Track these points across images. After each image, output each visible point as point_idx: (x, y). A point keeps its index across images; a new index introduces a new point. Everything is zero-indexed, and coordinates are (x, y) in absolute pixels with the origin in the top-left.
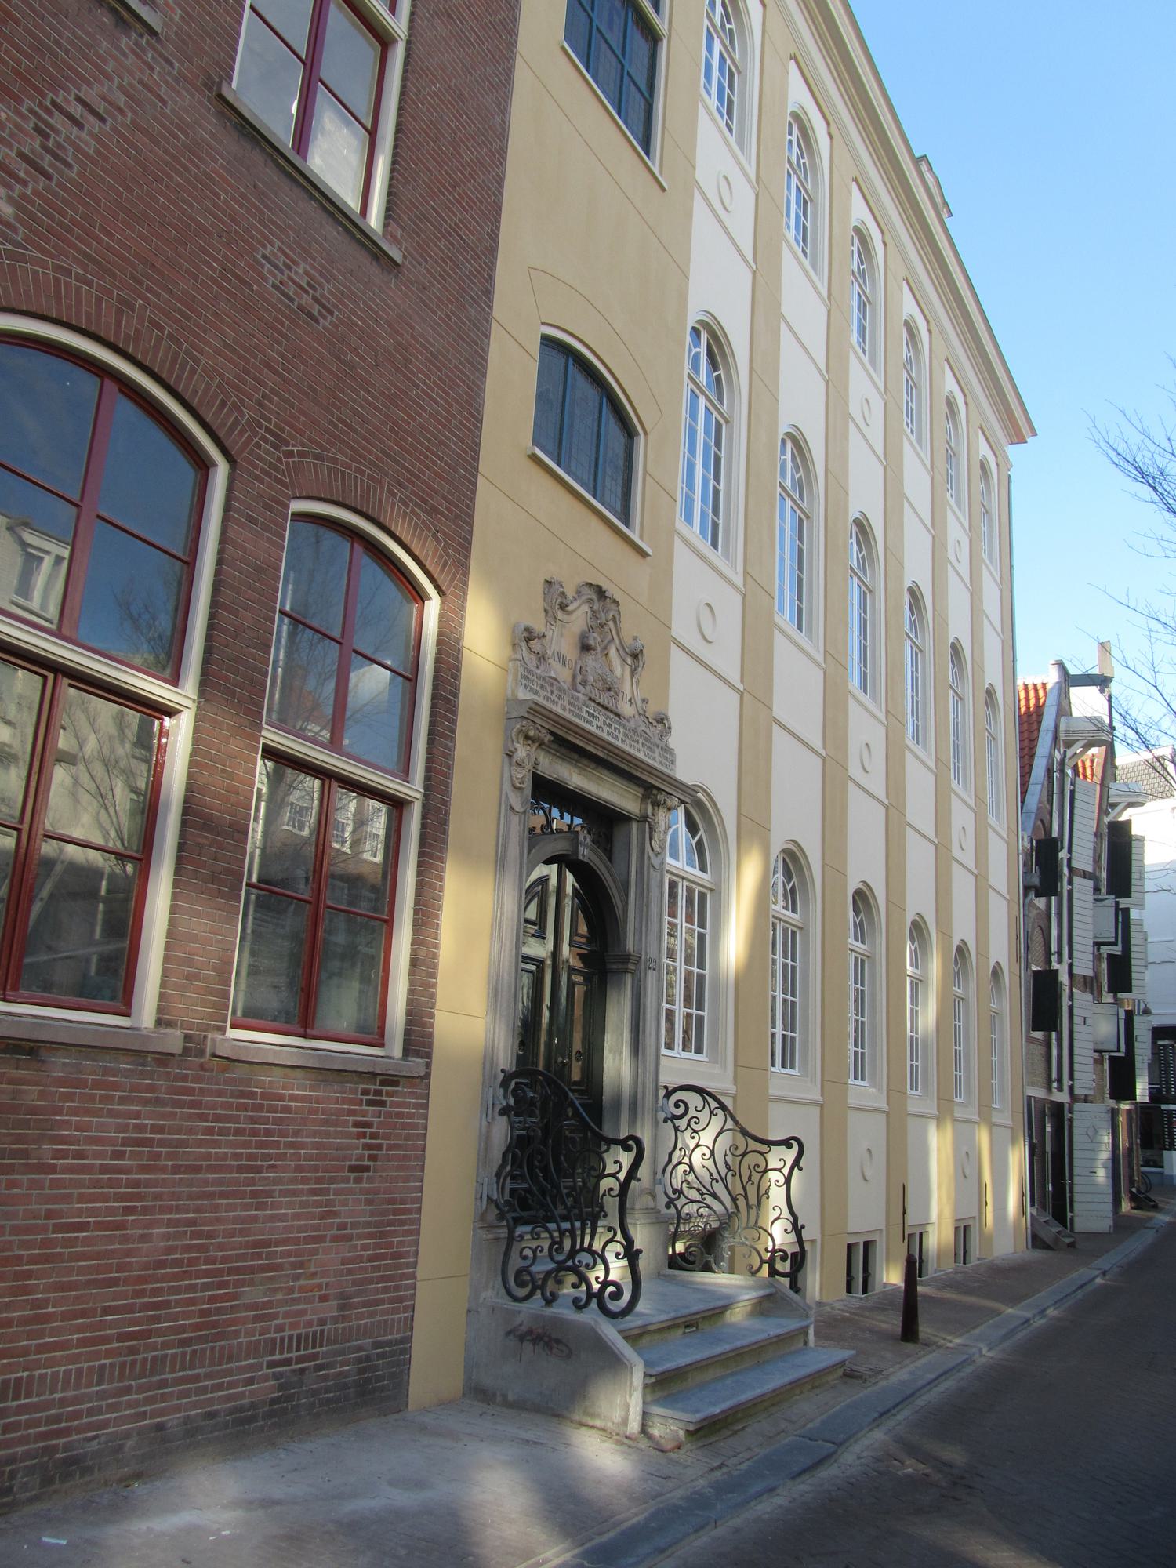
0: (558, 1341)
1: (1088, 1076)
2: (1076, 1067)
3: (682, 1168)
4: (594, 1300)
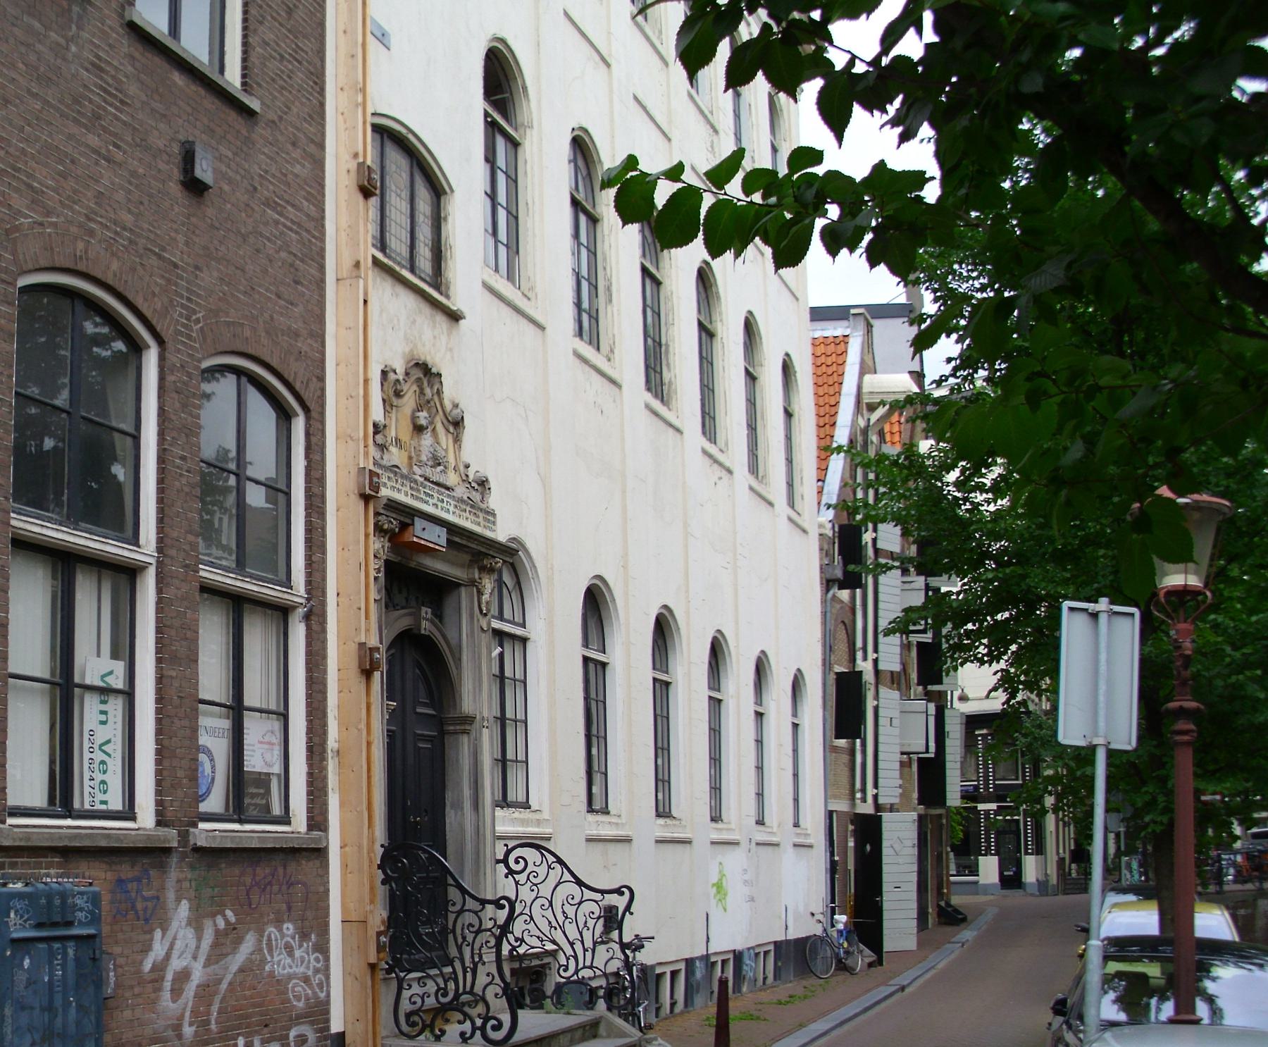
1: (892, 783)
2: (881, 773)
4: (478, 1032)
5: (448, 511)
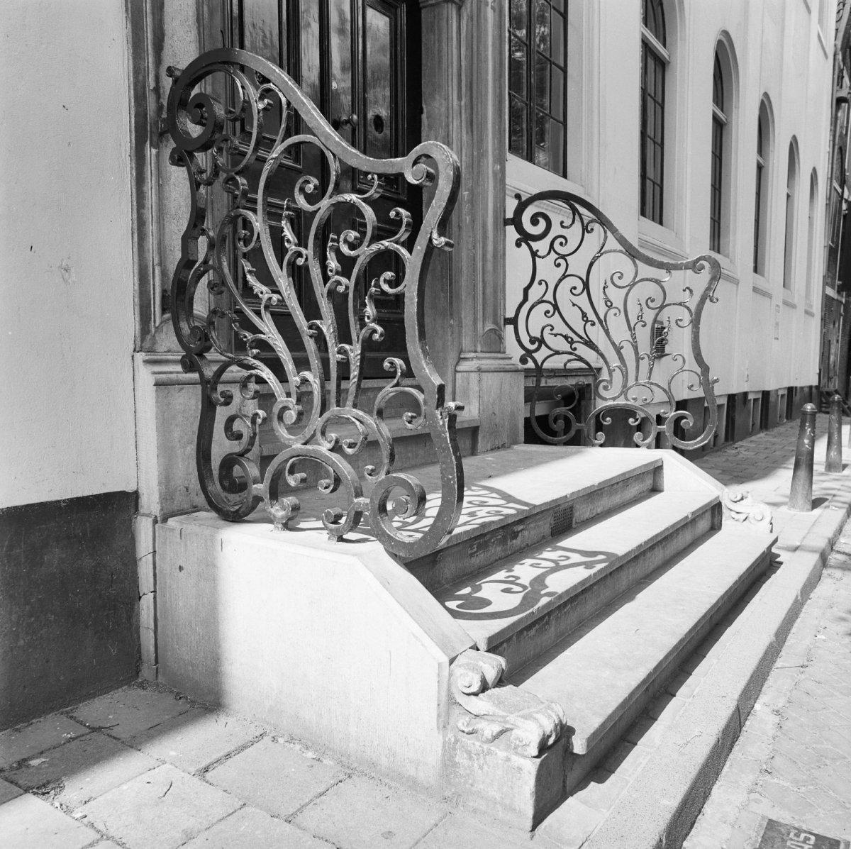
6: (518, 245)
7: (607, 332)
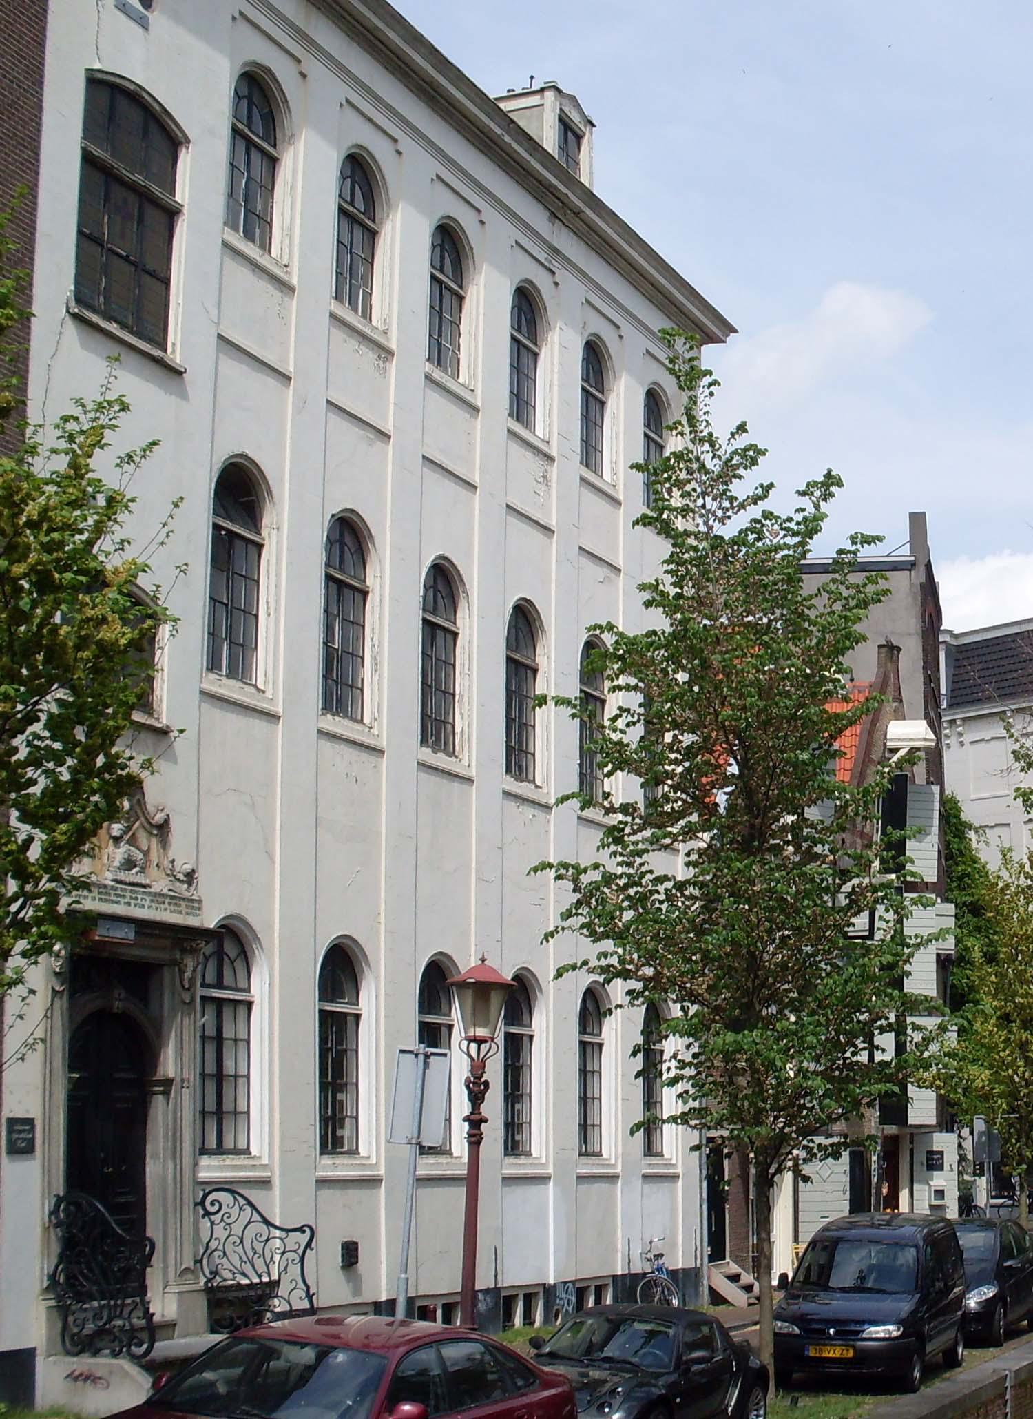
0: (100, 1378)
3: (216, 1254)
5: (143, 906)
6: (203, 1217)
7: (253, 1266)
